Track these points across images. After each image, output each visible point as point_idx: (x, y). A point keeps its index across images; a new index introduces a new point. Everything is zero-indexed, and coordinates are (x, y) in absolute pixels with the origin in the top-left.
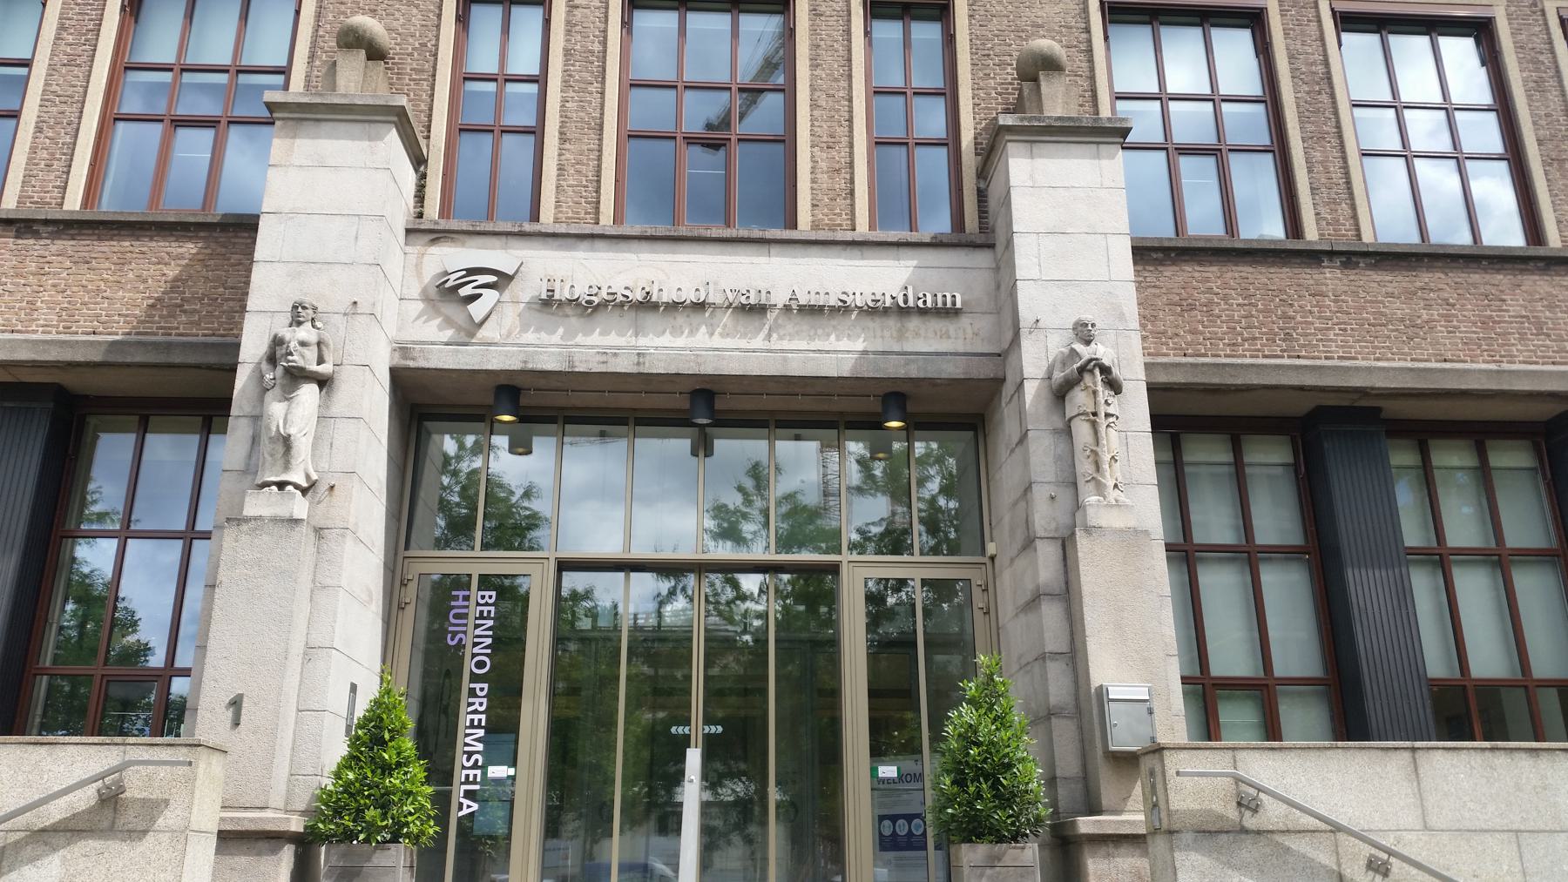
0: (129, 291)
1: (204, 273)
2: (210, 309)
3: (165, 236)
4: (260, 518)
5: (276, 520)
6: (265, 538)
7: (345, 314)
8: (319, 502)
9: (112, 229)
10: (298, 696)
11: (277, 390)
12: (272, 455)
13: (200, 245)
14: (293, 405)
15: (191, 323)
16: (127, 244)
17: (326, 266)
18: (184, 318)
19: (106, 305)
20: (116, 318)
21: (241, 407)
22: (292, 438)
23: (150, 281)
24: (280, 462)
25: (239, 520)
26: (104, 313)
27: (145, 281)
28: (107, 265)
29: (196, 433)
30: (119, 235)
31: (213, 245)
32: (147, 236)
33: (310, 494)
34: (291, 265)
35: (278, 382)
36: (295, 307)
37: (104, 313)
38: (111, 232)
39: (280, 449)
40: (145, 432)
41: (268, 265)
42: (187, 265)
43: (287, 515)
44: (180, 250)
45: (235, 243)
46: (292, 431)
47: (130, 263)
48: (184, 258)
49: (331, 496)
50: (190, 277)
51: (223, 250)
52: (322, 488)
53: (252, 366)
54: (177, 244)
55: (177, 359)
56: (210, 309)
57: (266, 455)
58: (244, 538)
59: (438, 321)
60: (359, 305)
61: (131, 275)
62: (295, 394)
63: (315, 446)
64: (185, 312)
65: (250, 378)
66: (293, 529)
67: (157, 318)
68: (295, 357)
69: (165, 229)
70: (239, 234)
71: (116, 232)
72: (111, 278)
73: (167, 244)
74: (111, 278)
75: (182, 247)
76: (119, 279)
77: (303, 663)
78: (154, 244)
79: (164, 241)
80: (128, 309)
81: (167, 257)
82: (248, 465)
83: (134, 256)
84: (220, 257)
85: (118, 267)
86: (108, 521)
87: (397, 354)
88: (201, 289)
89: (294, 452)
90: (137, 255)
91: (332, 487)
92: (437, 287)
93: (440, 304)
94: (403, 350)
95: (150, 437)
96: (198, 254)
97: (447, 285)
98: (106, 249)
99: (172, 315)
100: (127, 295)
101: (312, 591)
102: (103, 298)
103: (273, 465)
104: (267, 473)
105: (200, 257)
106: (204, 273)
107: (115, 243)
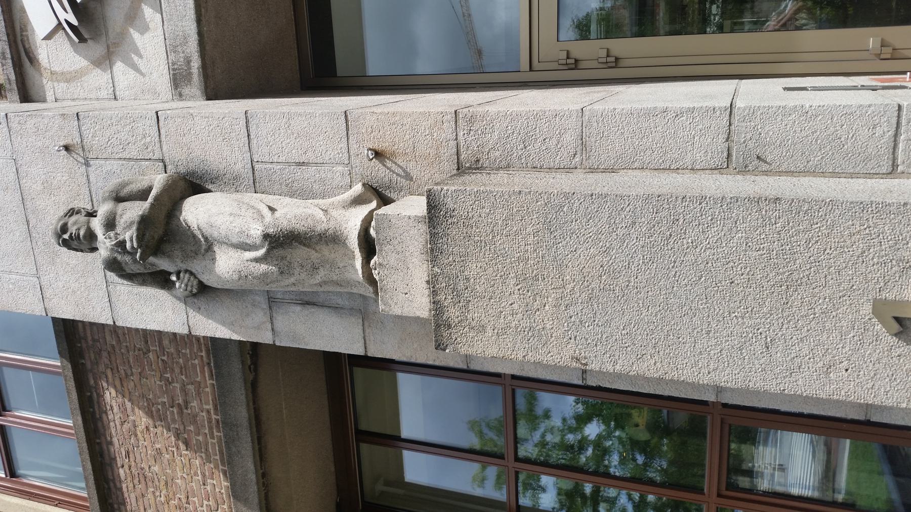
0: (174, 471)
1: (136, 378)
2: (177, 370)
3: (104, 427)
4: (432, 282)
5: (434, 252)
6: (473, 269)
7: (87, 164)
8: (408, 177)
9: (109, 488)
10: (852, 176)
11: (196, 266)
12: (315, 268)
13: (105, 385)
14: (216, 234)
15: (199, 394)
16: (121, 471)
17: (29, 204)
18: (194, 404)
19: (196, 499)
20: (209, 488)
21: (258, 328)
22: (271, 231)
23: (158, 446)
24: (326, 251)
25: (438, 326)
26: (205, 502)
27: (159, 452)
28: (150, 496)
29: (396, 374)
30: (113, 480)
31: (102, 368)
32: (109, 450)
33: (387, 193)
34: (39, 258)
35: (183, 266)
36: (66, 244)
37: (205, 502)
38: (114, 490)
39: (299, 253)
40: (399, 439)
41: (47, 294)
42: (130, 400)
43: (424, 228)
44: (116, 409)
45: (94, 340)
46: (256, 231)
47: (142, 469)
48: (124, 404)
49: (393, 154)
50: (143, 396)
51: (105, 354)
52: (380, 172)
53: (192, 313)
54: (110, 412)
55: (242, 413)
56: (177, 370)
57: (318, 279)
58: (476, 314)
59: (135, 35)
60: (68, 141)
61: (156, 468)
62: (197, 233)
63: (293, 193)
64: (186, 403)
65: (209, 316)
66: (450, 213)
67: (200, 438)
68: (127, 236)
69: (96, 430)
70: (82, 334)
71: (112, 485)
72: (164, 492)
73: (112, 424)
74: (164, 492)
75: (112, 407)
76: (163, 483)
77: (766, 173)
78: (115, 440)
79: (109, 428)
80: (196, 474)
81: (126, 426)
82: (352, 311)
83: (133, 463)
84: (113, 359)
85: (150, 484)
86: (597, 419)
87: (186, 91)
88: (154, 382)
89: (300, 227)
90: (132, 459)
91: (378, 155)
92: (82, 39)
93: (112, 35)
94: (178, 79)
95: (405, 433)
96: (115, 387)
97: (75, 22)
98: (133, 496)
99: (194, 418)
100: (179, 474)
101: (592, 170)
102: (188, 503)
103: (333, 265)
104: (349, 275)
105: (118, 383)
106: (136, 378)
107: (124, 486)
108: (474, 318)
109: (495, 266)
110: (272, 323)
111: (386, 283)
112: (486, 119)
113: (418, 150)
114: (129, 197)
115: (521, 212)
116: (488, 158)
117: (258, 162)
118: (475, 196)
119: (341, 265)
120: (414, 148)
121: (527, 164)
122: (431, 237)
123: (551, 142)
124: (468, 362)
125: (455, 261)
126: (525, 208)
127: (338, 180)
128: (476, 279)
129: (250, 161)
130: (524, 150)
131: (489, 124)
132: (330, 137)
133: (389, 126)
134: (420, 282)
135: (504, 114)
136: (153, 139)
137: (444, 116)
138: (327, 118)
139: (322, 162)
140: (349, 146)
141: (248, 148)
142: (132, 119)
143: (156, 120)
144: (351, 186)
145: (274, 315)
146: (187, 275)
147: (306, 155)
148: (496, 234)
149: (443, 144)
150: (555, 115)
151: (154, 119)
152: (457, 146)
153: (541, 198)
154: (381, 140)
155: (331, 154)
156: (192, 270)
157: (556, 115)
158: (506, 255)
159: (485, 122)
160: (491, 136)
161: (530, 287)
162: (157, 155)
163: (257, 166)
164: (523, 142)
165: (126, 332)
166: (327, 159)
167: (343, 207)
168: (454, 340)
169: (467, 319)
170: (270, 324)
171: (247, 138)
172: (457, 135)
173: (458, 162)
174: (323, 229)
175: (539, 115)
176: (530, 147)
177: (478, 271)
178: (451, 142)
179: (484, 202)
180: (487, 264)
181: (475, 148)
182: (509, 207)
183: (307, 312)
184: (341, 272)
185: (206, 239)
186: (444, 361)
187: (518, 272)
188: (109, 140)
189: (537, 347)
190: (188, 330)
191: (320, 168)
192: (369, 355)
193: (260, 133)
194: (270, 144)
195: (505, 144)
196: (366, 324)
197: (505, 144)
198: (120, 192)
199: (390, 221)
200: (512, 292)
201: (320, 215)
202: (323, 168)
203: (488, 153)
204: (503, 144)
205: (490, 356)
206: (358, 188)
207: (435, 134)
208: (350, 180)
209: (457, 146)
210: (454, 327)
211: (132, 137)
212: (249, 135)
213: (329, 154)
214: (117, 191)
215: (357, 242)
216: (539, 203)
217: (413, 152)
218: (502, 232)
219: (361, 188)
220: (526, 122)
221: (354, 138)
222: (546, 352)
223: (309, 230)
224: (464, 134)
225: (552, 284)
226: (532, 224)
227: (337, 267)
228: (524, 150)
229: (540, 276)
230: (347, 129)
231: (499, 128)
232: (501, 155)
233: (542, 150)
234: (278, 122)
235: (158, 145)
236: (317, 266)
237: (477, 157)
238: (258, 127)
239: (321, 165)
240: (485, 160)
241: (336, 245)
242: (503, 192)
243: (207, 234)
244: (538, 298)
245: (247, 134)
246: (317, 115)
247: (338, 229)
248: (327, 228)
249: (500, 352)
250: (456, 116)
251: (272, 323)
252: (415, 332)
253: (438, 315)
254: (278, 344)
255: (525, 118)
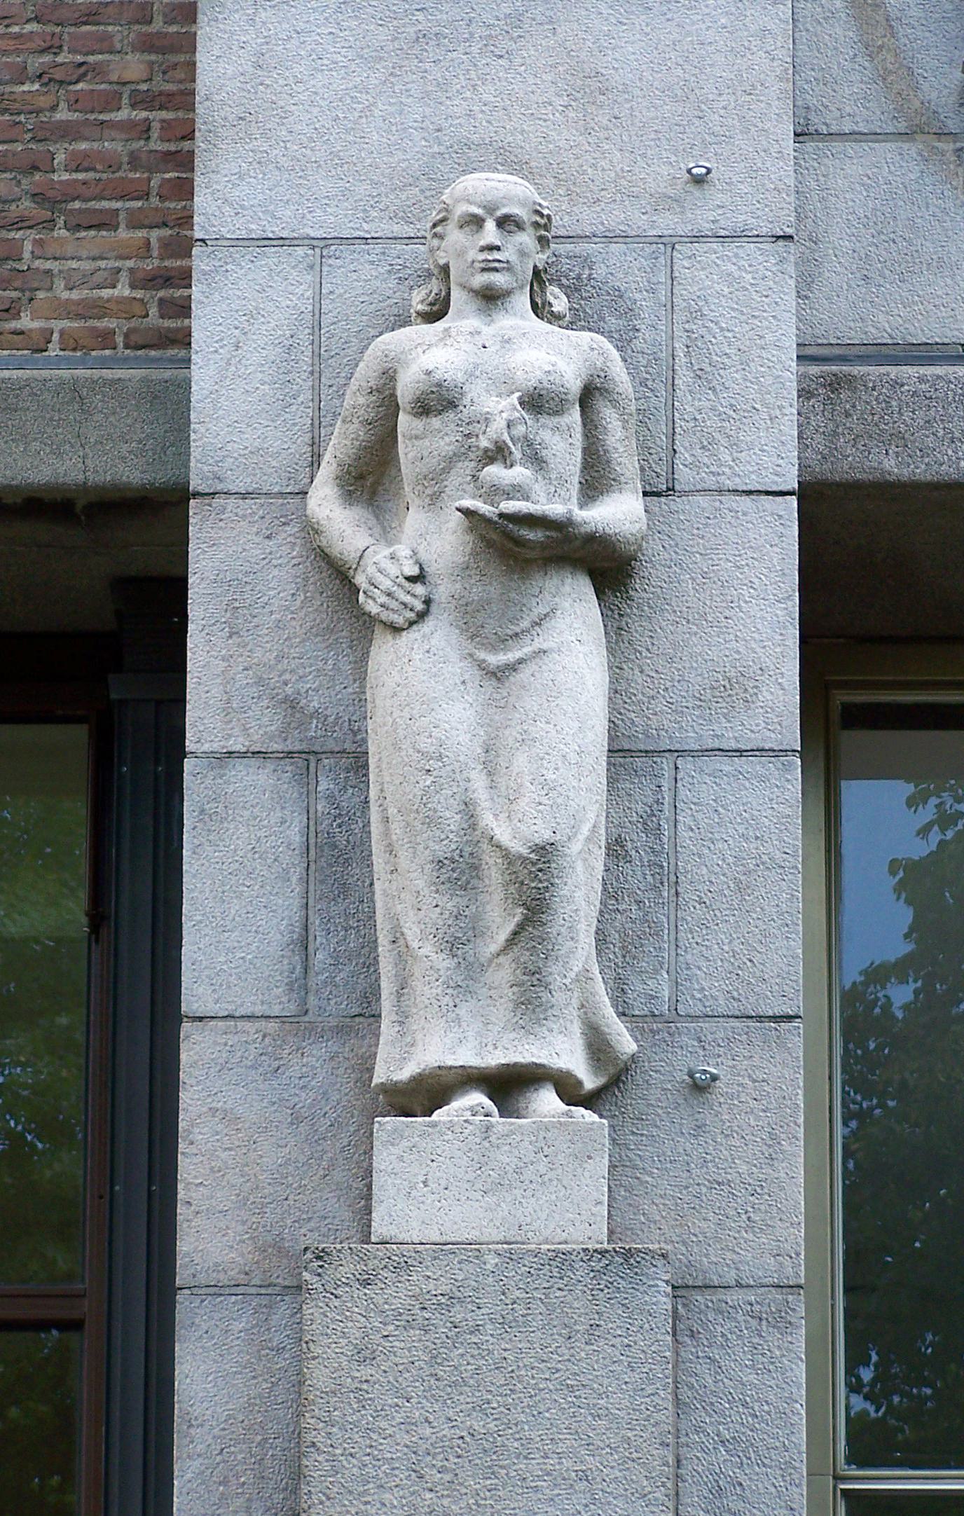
14: (531, 703)
24: (503, 974)
91: (700, 1087)
108: (390, 1339)
109: (510, 1390)
110: (243, 755)
111: (446, 1138)
112: (784, 1356)
113: (714, 1191)
114: (592, 421)
115: (626, 1446)
116: (698, 1357)
117: (677, 768)
118: (654, 1352)
119: (463, 1011)
120: (719, 1184)
121: (688, 1446)
122: (563, 1254)
123: (735, 1498)
124: (195, 1291)
125: (515, 1302)
126: (635, 1455)
127: (636, 987)
128: (479, 1348)
129: (678, 747)
130: (716, 1438)
131: (772, 1363)
132: (740, 972)
133: (769, 1124)
134: (456, 1219)
135: (794, 1396)
136: (727, 470)
137: (791, 1257)
138: (786, 969)
139: (680, 944)
140: (721, 1020)
141: (710, 747)
142: (778, 412)
143: (775, 488)
144: (624, 1015)
145: (270, 766)
146: (419, 606)
147: (696, 904)
148: (577, 1393)
149: (729, 1255)
150: (794, 1506)
151: (776, 483)
152: (725, 1287)
153: (658, 1487)
154: (736, 1102)
155: (699, 969)
156: (431, 618)
157: (791, 1509)
158: (535, 1413)
159: (778, 1353)
160: (746, 1366)
161: (470, 1461)
162: (685, 476)
163: (666, 764)
164: (734, 1438)
165: (15, 29)
166: (689, 956)
167: (583, 1006)
168: (334, 1291)
169: (385, 1324)
170: (244, 750)
171: (734, 745)
172: (749, 1286)
173: (687, 1287)
174: (550, 979)
175: (793, 1471)
176: (724, 1453)
177: (496, 1352)
178: (733, 1273)
179: (644, 1370)
180: (513, 1371)
181: (719, 1329)
182: (635, 1422)
183: (285, 860)
184: (444, 1009)
185: (513, 667)
186: (189, 1226)
187: (499, 1436)
188: (722, 329)
189: (337, 1473)
190: (200, 489)
191: (666, 937)
192: (186, 1027)
193: (747, 785)
194: (720, 809)
195: (730, 1398)
196: (272, 1026)
197: (730, 1398)
198: (601, 394)
199: (590, 1157)
200: (454, 1423)
201: (577, 966)
202: (666, 946)
203: (710, 1358)
204: (731, 1393)
205: (305, 1370)
206: (626, 1043)
207: (751, 1236)
208: (637, 1013)
209: (725, 1287)
210: (365, 1294)
211: (731, 405)
212: (740, 752)
213: (701, 964)
214: (606, 390)
215: (522, 1060)
216: (645, 1483)
217: (709, 1181)
218: (582, 1405)
219: (627, 1050)
220: (778, 1444)
221: (740, 1035)
222: (328, 1491)
223: (551, 947)
224: (751, 1305)
225: (479, 1505)
226: (602, 1467)
227: (457, 1001)
228: (716, 1438)
229: (493, 1482)
230: (760, 1018)
231: (764, 1384)
232: (705, 1387)
233: (717, 1478)
234: (774, 837)
235: (711, 482)
236: (459, 952)
237: (699, 1333)
238: (763, 779)
239: (673, 942)
240: (693, 1350)
241: (511, 1005)
242: (665, 1411)
243: (524, 675)
244: (448, 1477)
245: (744, 748)
246: (792, 943)
247: (549, 1013)
248: (551, 987)
249: (318, 1393)
250: (792, 1287)
251: (243, 755)
252: (261, 1157)
253: (389, 1258)
254: (188, 764)
255: (786, 1443)
